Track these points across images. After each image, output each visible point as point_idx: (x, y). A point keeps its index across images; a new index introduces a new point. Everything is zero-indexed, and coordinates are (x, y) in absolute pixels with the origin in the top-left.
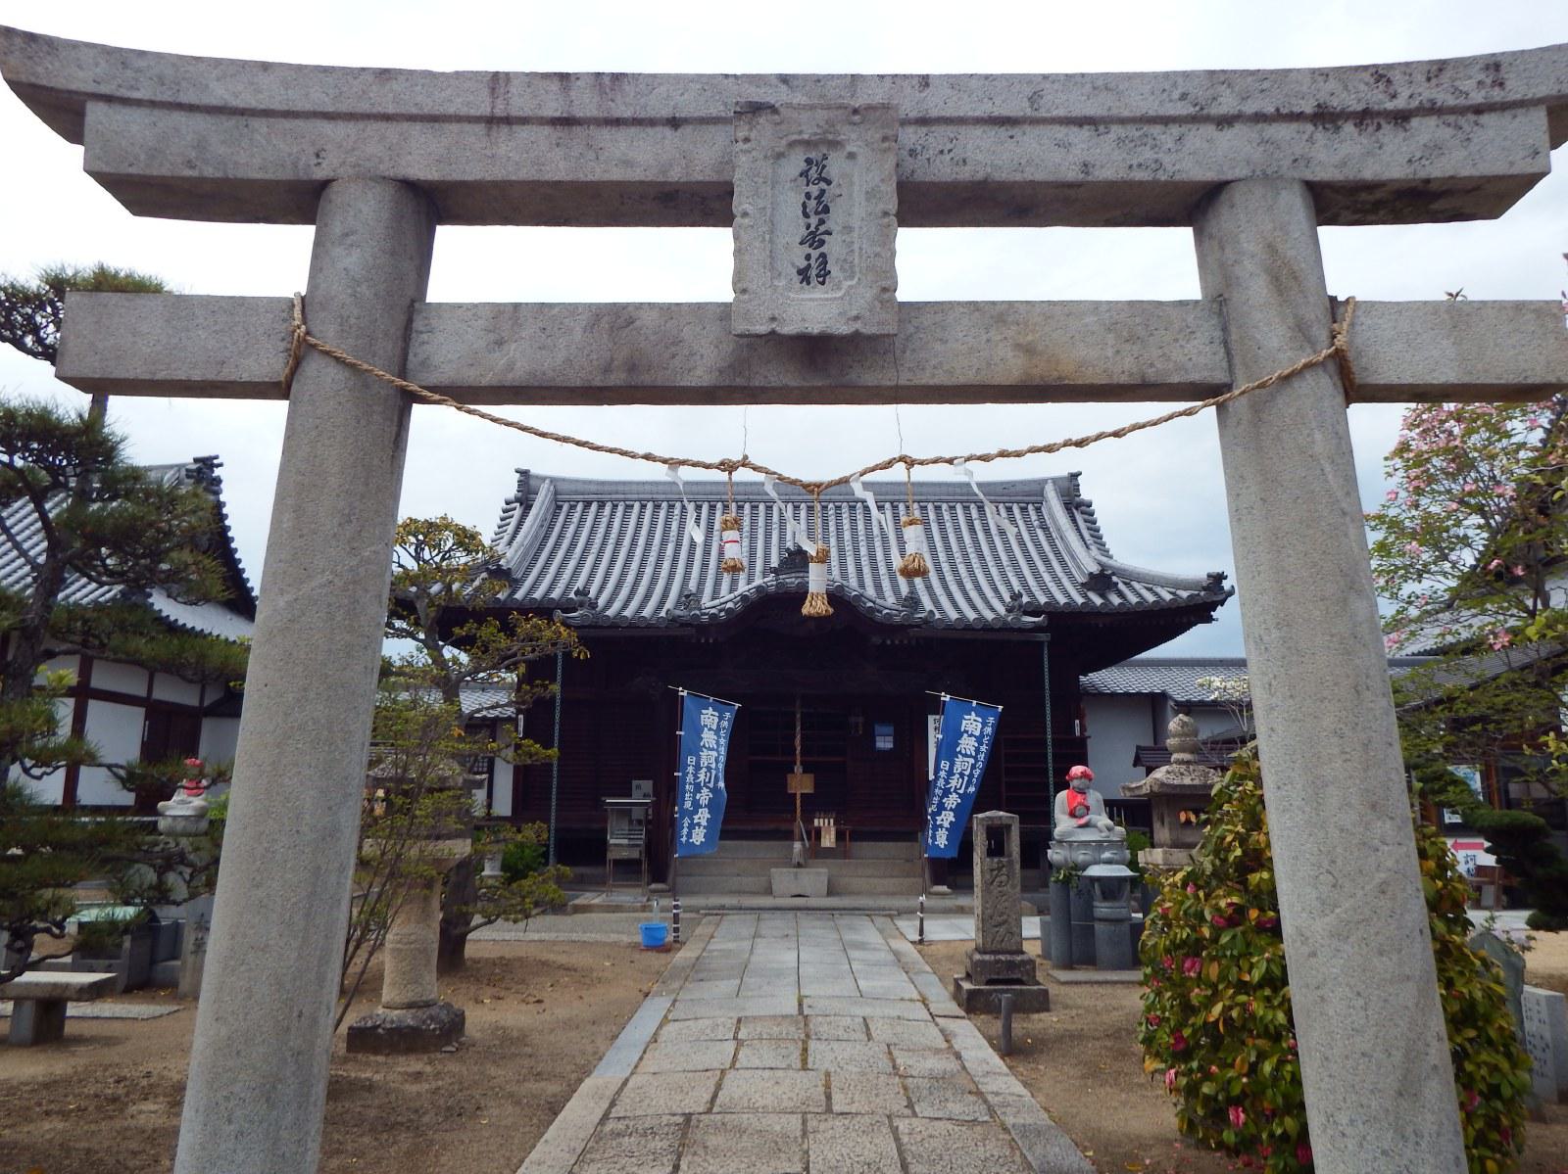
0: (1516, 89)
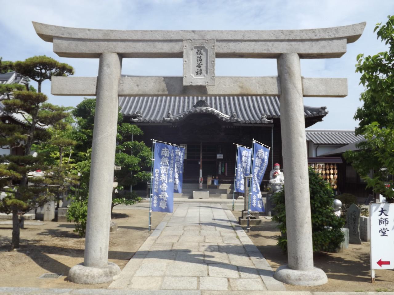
0: (341, 35)
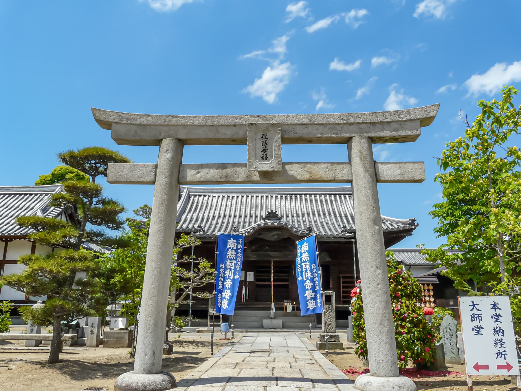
0: (413, 117)
